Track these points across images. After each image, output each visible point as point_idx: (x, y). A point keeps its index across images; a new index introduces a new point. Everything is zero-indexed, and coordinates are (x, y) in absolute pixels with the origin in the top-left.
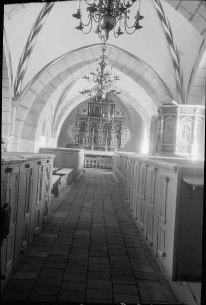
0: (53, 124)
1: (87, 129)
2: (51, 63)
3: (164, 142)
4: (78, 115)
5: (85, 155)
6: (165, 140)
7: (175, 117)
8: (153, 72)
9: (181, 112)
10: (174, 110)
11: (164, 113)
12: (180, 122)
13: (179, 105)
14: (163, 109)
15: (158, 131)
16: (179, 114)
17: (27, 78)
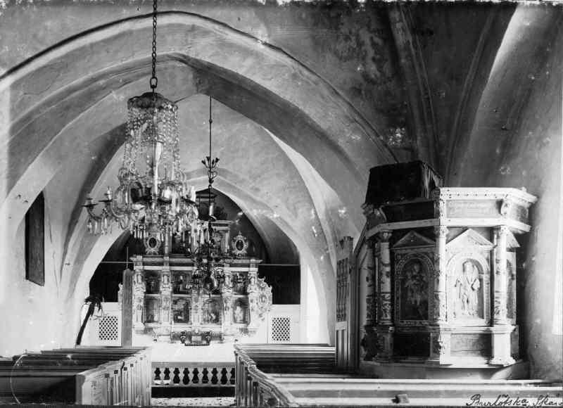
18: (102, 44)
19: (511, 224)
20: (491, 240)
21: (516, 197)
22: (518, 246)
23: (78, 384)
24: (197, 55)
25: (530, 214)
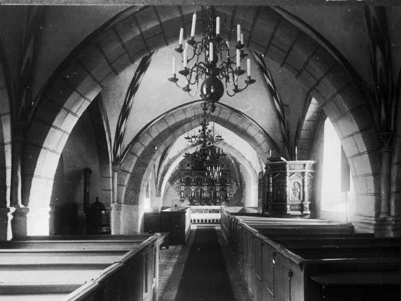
0: (156, 183)
2: (151, 123)
3: (274, 201)
4: (182, 170)
5: (175, 50)
7: (284, 175)
8: (258, 126)
9: (290, 169)
10: (283, 166)
11: (272, 170)
13: (288, 162)
15: (267, 189)
16: (288, 171)
17: (127, 140)
18: (34, 292)
19: (308, 170)
20: (322, 110)
21: (309, 163)
22: (328, 118)
23: (179, 277)
24: (51, 179)
25: (315, 167)
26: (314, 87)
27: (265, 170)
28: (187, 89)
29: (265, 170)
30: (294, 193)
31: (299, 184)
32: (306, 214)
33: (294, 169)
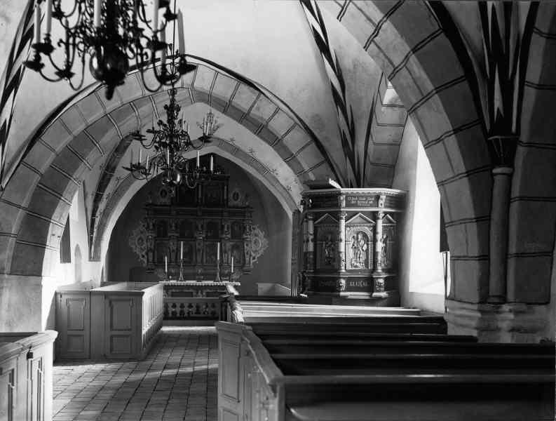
1: (169, 234)
3: (316, 271)
6: (318, 267)
9: (348, 205)
12: (346, 226)
13: (344, 190)
14: (314, 197)
26: (372, 40)
27: (302, 206)
28: (66, 73)
29: (302, 206)
30: (355, 254)
31: (365, 236)
32: (380, 299)
33: (356, 205)
